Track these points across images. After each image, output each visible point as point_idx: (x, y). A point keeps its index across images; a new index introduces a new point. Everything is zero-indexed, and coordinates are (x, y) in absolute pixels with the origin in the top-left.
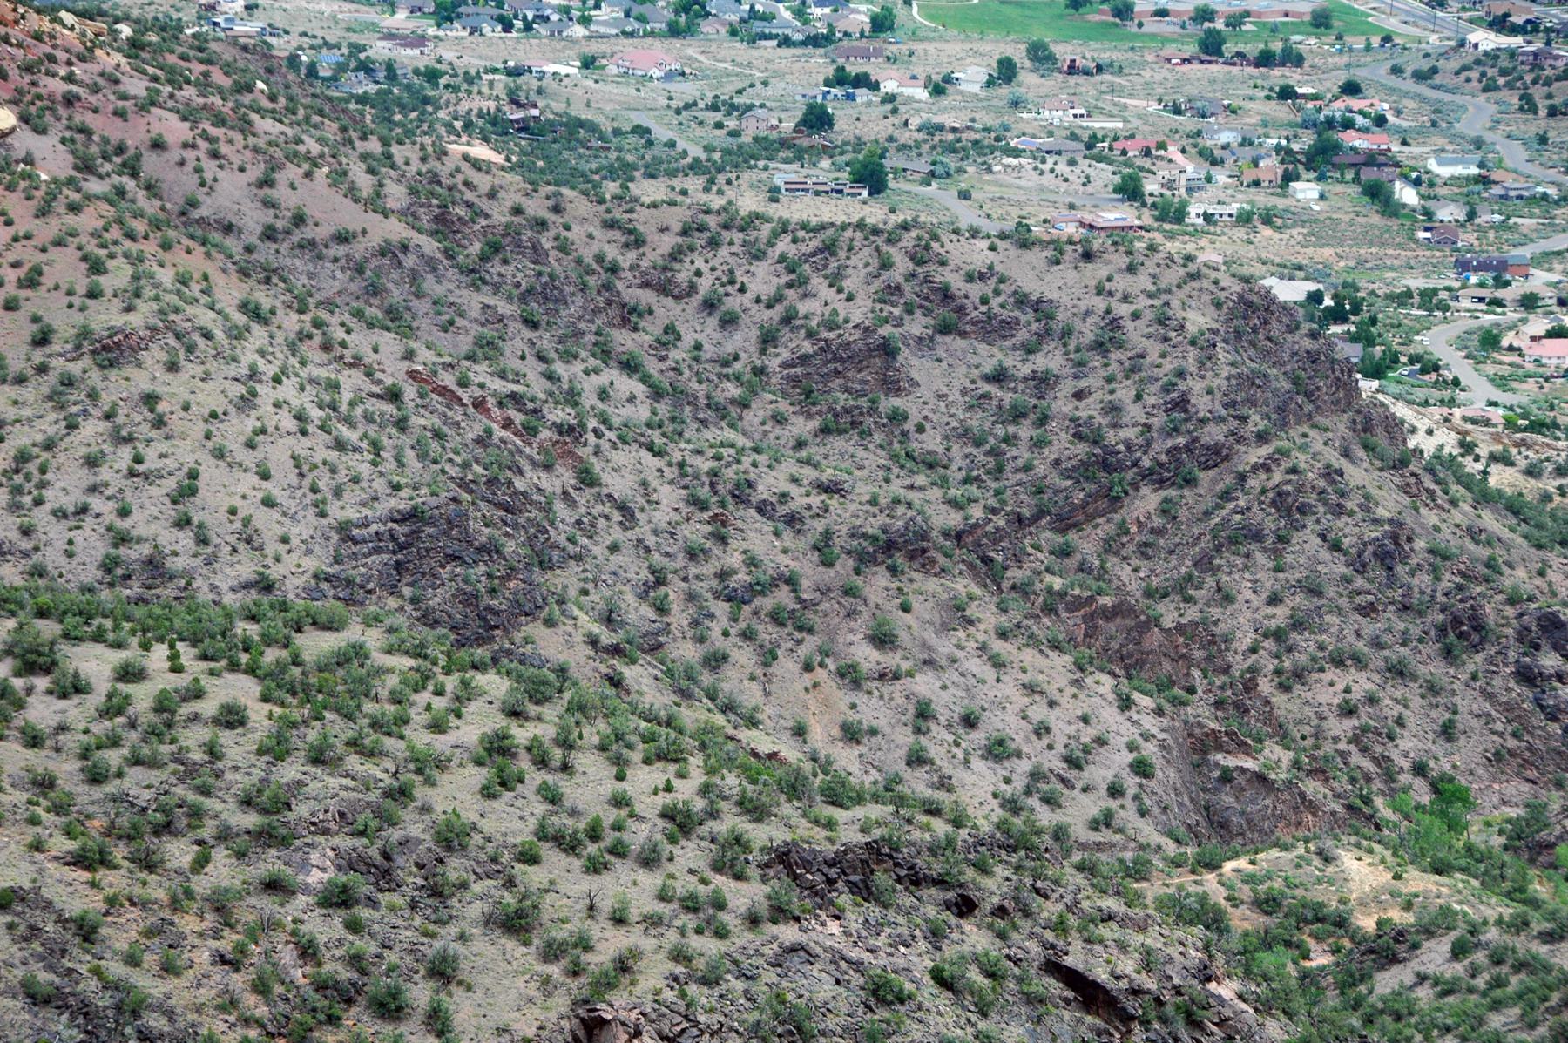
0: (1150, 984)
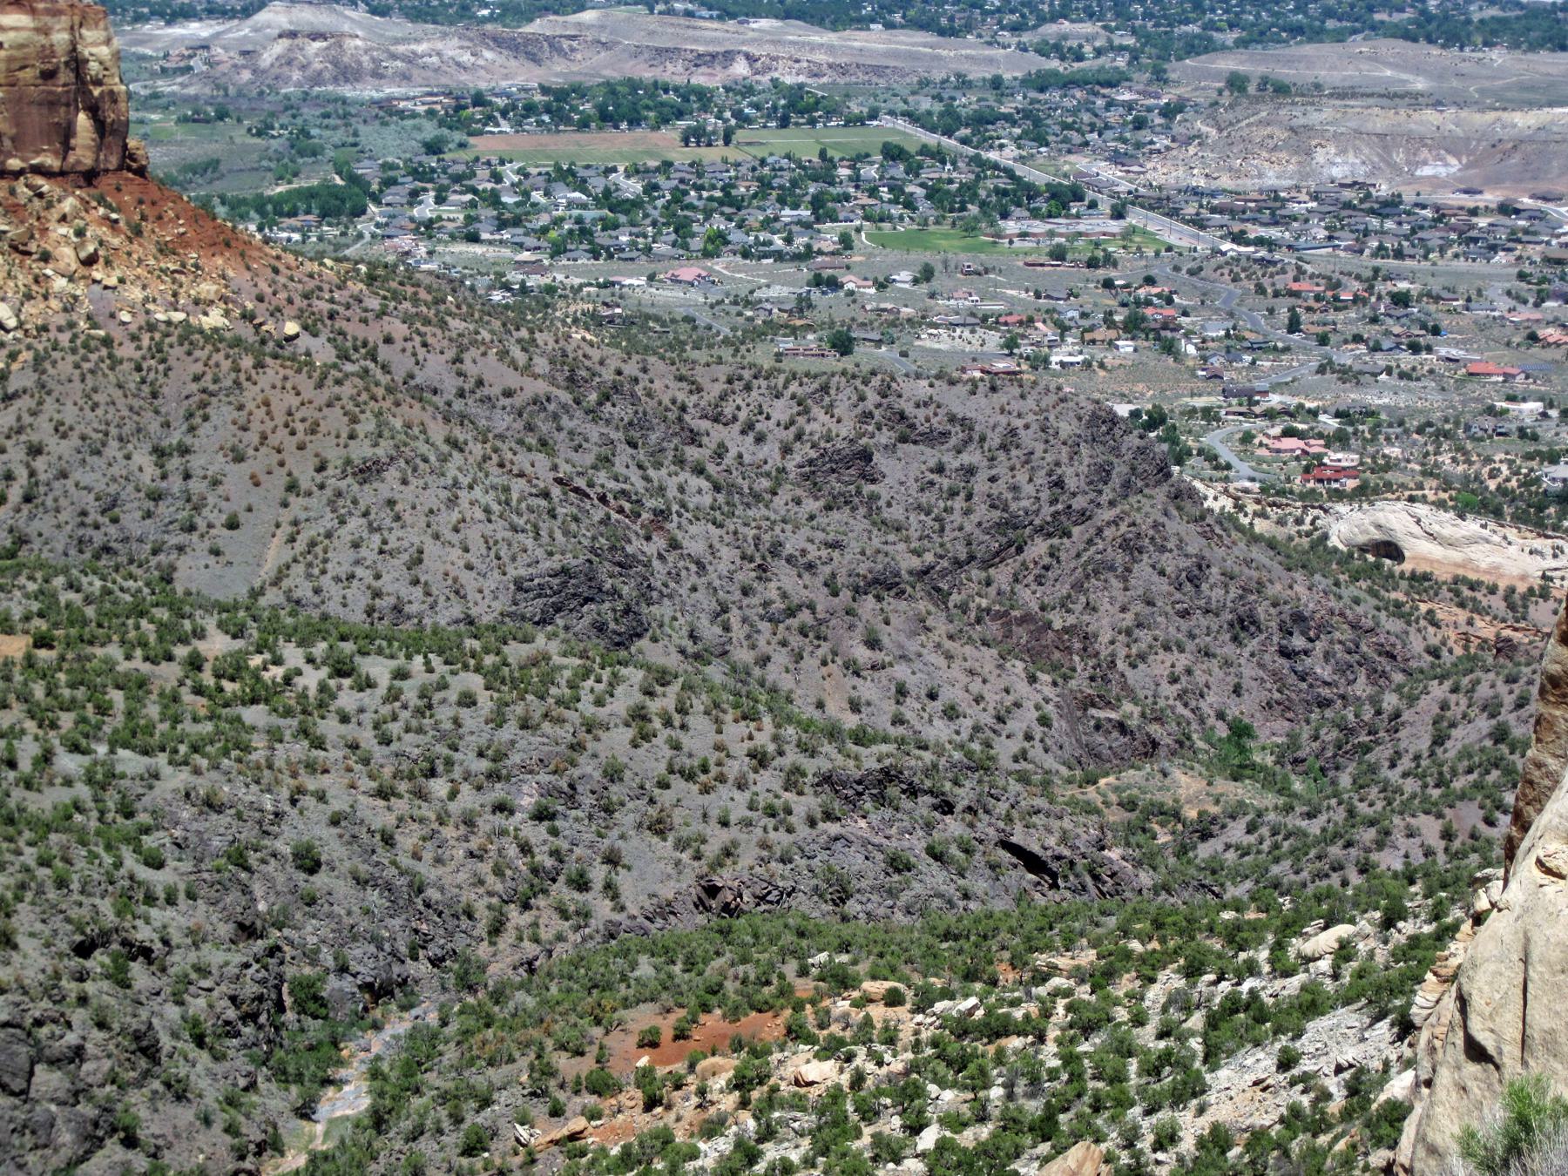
0: (1066, 852)
